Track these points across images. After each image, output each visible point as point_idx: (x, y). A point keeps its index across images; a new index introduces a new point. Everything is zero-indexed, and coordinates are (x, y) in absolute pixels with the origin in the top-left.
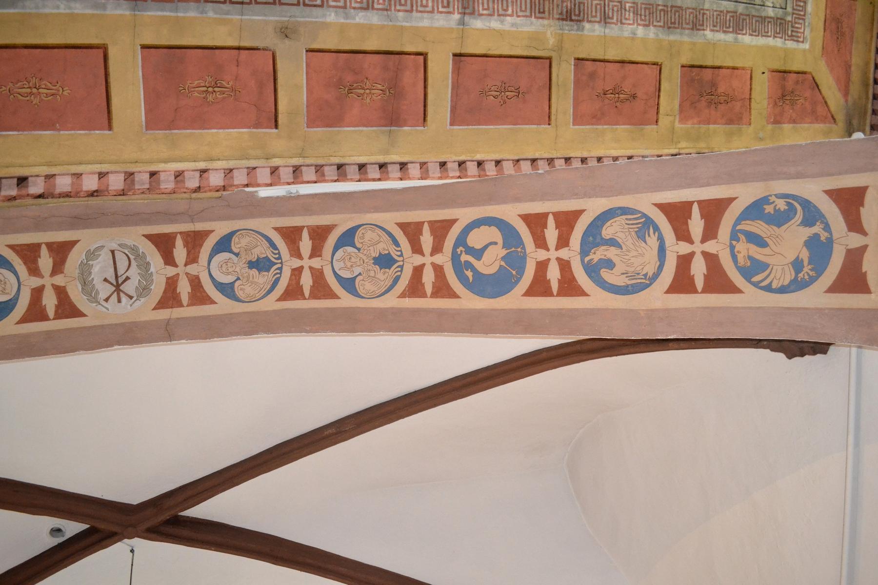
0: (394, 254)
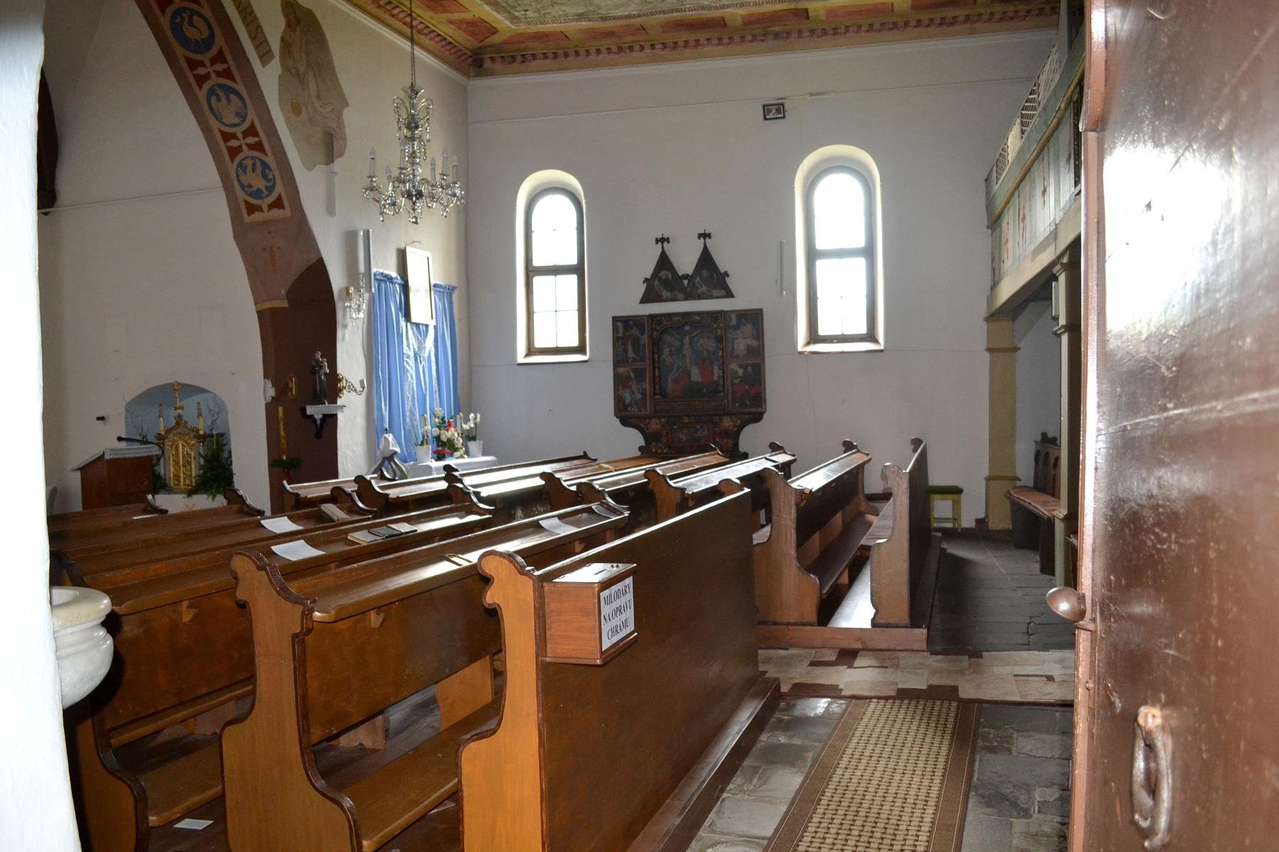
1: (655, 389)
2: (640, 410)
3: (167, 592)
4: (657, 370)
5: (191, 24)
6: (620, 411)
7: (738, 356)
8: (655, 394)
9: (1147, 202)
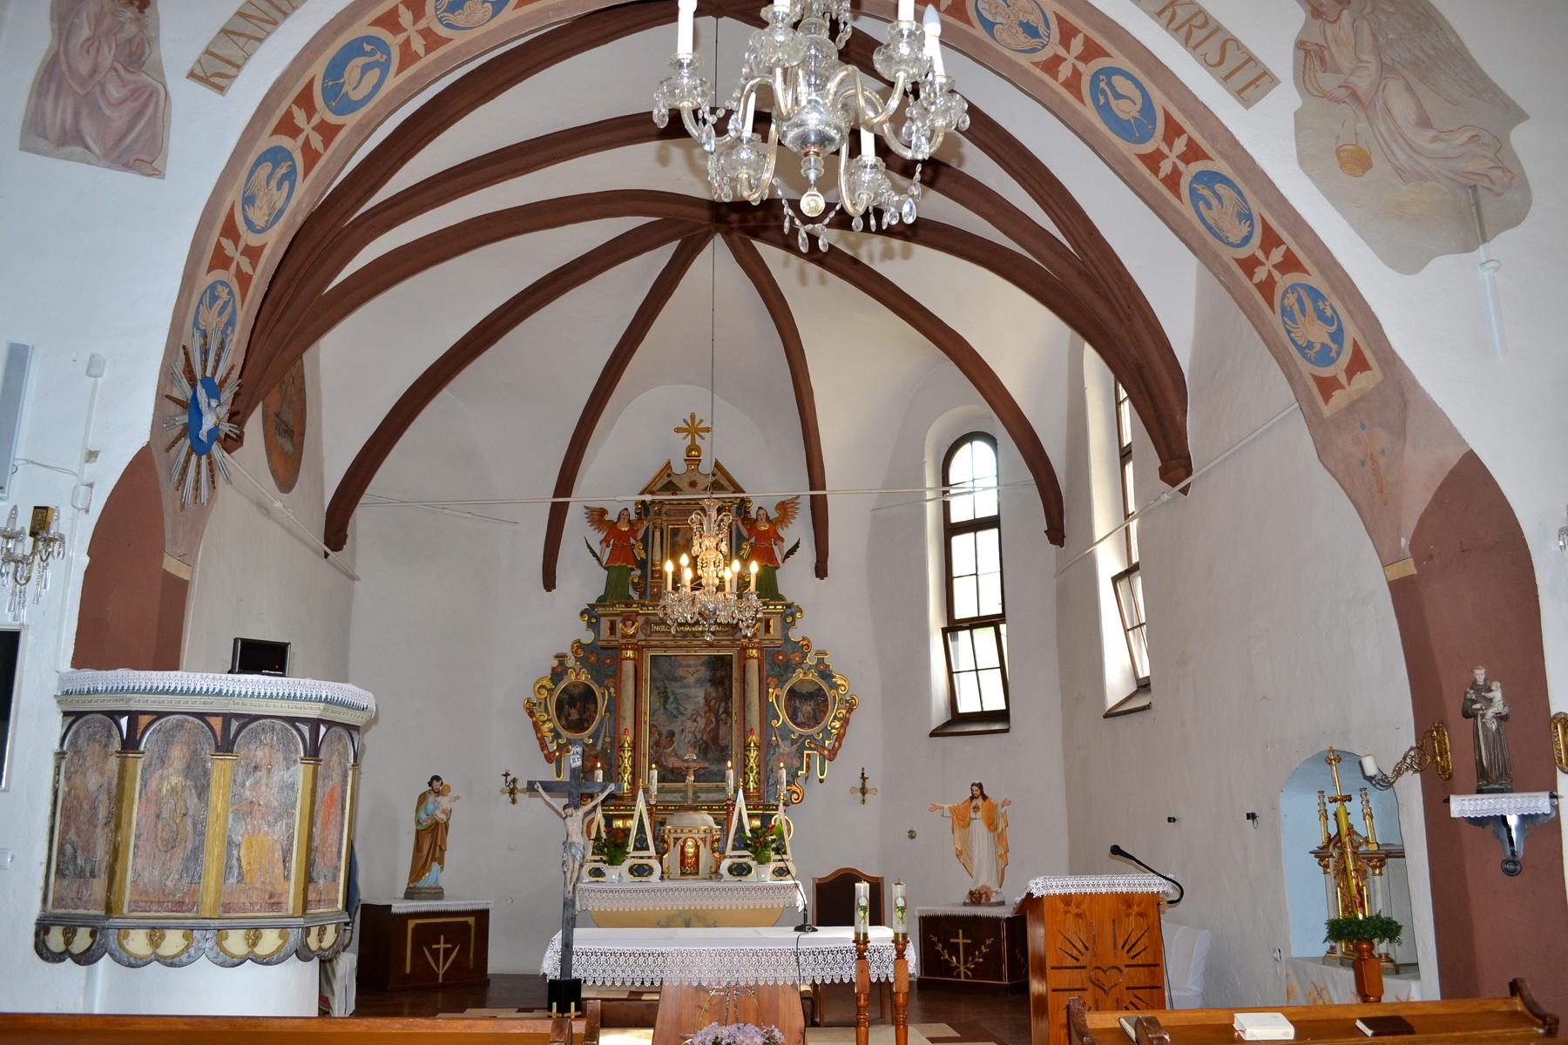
0: (1041, 30)
5: (365, 69)
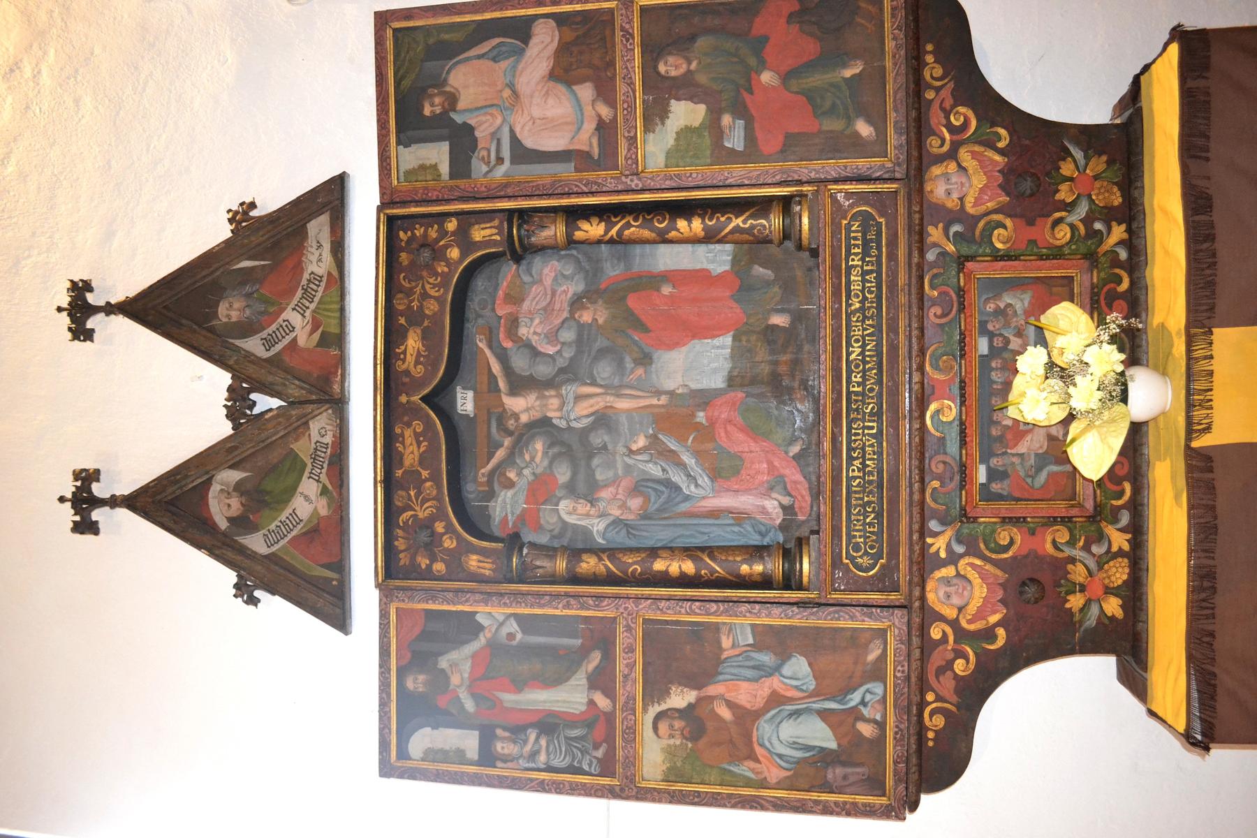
1: (765, 582)
2: (877, 673)
3: (514, 560)
4: (659, 566)
6: (875, 784)
7: (605, 130)
8: (790, 581)
9: (90, 465)
